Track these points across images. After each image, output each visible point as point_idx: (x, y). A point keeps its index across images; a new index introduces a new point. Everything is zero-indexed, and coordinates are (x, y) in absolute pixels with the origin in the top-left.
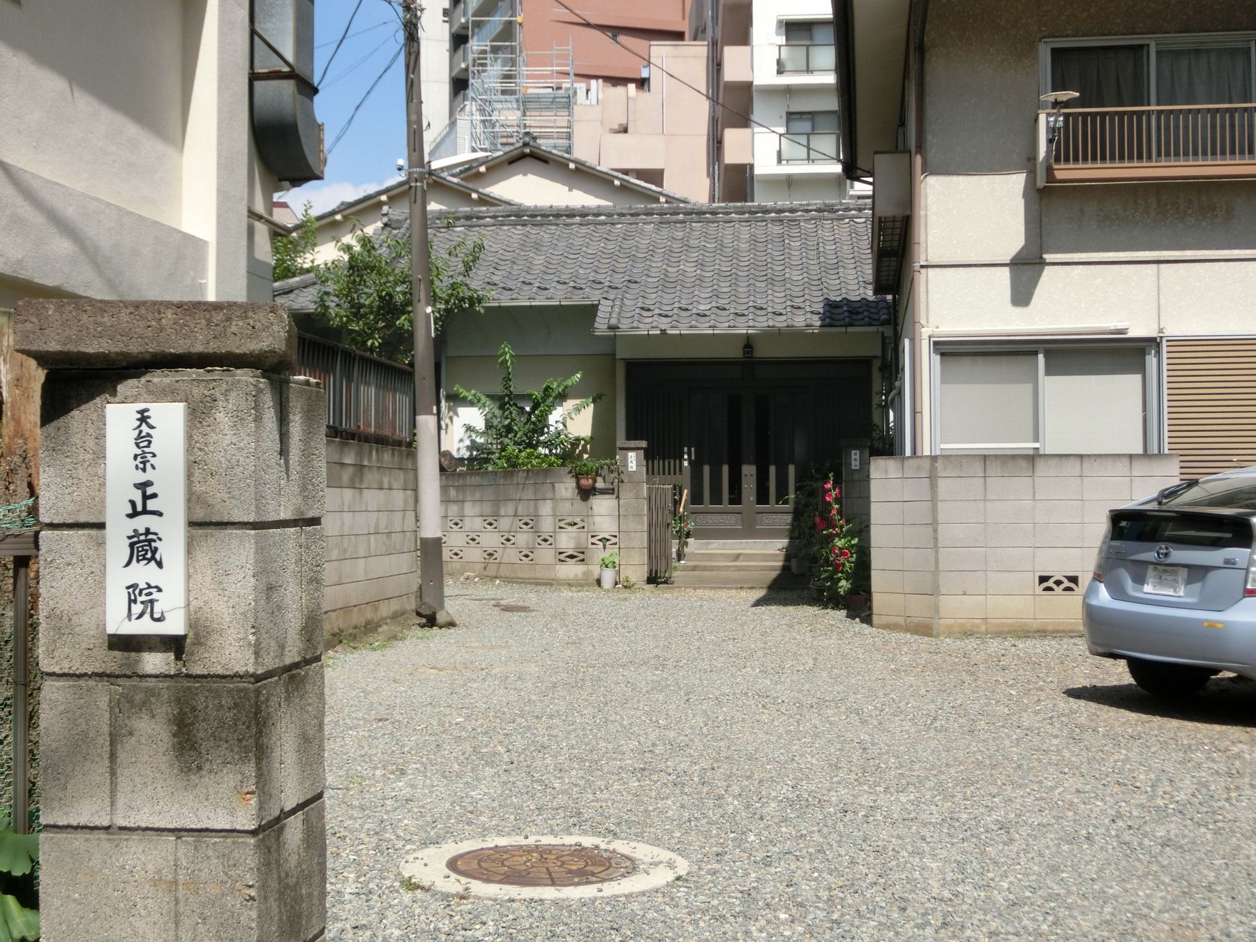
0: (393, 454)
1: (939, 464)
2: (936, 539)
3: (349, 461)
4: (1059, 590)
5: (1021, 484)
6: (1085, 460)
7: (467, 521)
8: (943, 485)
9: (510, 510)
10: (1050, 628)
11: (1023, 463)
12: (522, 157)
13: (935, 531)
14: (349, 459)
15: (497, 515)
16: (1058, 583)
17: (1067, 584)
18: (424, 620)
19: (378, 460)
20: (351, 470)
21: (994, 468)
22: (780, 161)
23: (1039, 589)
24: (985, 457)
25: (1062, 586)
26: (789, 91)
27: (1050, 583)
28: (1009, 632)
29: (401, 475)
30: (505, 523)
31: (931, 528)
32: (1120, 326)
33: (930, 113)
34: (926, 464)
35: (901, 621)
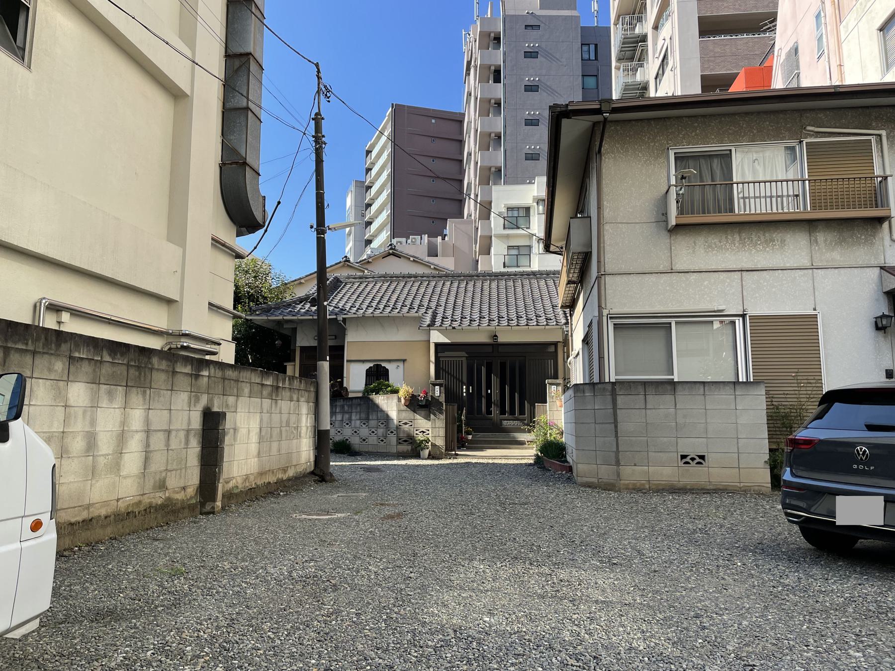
0: (301, 382)
1: (617, 387)
2: (616, 432)
3: (268, 383)
4: (693, 464)
5: (669, 398)
6: (706, 385)
7: (353, 422)
8: (620, 400)
9: (374, 417)
10: (689, 487)
11: (669, 387)
12: (390, 254)
13: (616, 427)
14: (269, 382)
15: (368, 419)
16: (693, 459)
17: (698, 460)
18: (317, 478)
19: (290, 384)
20: (270, 389)
21: (650, 390)
22: (504, 267)
23: (681, 464)
24: (645, 382)
25: (696, 461)
26: (508, 237)
27: (688, 459)
28: (663, 489)
29: (306, 394)
30: (373, 423)
31: (151, 448)
32: (721, 308)
33: (605, 189)
34: (609, 387)
35: (595, 480)
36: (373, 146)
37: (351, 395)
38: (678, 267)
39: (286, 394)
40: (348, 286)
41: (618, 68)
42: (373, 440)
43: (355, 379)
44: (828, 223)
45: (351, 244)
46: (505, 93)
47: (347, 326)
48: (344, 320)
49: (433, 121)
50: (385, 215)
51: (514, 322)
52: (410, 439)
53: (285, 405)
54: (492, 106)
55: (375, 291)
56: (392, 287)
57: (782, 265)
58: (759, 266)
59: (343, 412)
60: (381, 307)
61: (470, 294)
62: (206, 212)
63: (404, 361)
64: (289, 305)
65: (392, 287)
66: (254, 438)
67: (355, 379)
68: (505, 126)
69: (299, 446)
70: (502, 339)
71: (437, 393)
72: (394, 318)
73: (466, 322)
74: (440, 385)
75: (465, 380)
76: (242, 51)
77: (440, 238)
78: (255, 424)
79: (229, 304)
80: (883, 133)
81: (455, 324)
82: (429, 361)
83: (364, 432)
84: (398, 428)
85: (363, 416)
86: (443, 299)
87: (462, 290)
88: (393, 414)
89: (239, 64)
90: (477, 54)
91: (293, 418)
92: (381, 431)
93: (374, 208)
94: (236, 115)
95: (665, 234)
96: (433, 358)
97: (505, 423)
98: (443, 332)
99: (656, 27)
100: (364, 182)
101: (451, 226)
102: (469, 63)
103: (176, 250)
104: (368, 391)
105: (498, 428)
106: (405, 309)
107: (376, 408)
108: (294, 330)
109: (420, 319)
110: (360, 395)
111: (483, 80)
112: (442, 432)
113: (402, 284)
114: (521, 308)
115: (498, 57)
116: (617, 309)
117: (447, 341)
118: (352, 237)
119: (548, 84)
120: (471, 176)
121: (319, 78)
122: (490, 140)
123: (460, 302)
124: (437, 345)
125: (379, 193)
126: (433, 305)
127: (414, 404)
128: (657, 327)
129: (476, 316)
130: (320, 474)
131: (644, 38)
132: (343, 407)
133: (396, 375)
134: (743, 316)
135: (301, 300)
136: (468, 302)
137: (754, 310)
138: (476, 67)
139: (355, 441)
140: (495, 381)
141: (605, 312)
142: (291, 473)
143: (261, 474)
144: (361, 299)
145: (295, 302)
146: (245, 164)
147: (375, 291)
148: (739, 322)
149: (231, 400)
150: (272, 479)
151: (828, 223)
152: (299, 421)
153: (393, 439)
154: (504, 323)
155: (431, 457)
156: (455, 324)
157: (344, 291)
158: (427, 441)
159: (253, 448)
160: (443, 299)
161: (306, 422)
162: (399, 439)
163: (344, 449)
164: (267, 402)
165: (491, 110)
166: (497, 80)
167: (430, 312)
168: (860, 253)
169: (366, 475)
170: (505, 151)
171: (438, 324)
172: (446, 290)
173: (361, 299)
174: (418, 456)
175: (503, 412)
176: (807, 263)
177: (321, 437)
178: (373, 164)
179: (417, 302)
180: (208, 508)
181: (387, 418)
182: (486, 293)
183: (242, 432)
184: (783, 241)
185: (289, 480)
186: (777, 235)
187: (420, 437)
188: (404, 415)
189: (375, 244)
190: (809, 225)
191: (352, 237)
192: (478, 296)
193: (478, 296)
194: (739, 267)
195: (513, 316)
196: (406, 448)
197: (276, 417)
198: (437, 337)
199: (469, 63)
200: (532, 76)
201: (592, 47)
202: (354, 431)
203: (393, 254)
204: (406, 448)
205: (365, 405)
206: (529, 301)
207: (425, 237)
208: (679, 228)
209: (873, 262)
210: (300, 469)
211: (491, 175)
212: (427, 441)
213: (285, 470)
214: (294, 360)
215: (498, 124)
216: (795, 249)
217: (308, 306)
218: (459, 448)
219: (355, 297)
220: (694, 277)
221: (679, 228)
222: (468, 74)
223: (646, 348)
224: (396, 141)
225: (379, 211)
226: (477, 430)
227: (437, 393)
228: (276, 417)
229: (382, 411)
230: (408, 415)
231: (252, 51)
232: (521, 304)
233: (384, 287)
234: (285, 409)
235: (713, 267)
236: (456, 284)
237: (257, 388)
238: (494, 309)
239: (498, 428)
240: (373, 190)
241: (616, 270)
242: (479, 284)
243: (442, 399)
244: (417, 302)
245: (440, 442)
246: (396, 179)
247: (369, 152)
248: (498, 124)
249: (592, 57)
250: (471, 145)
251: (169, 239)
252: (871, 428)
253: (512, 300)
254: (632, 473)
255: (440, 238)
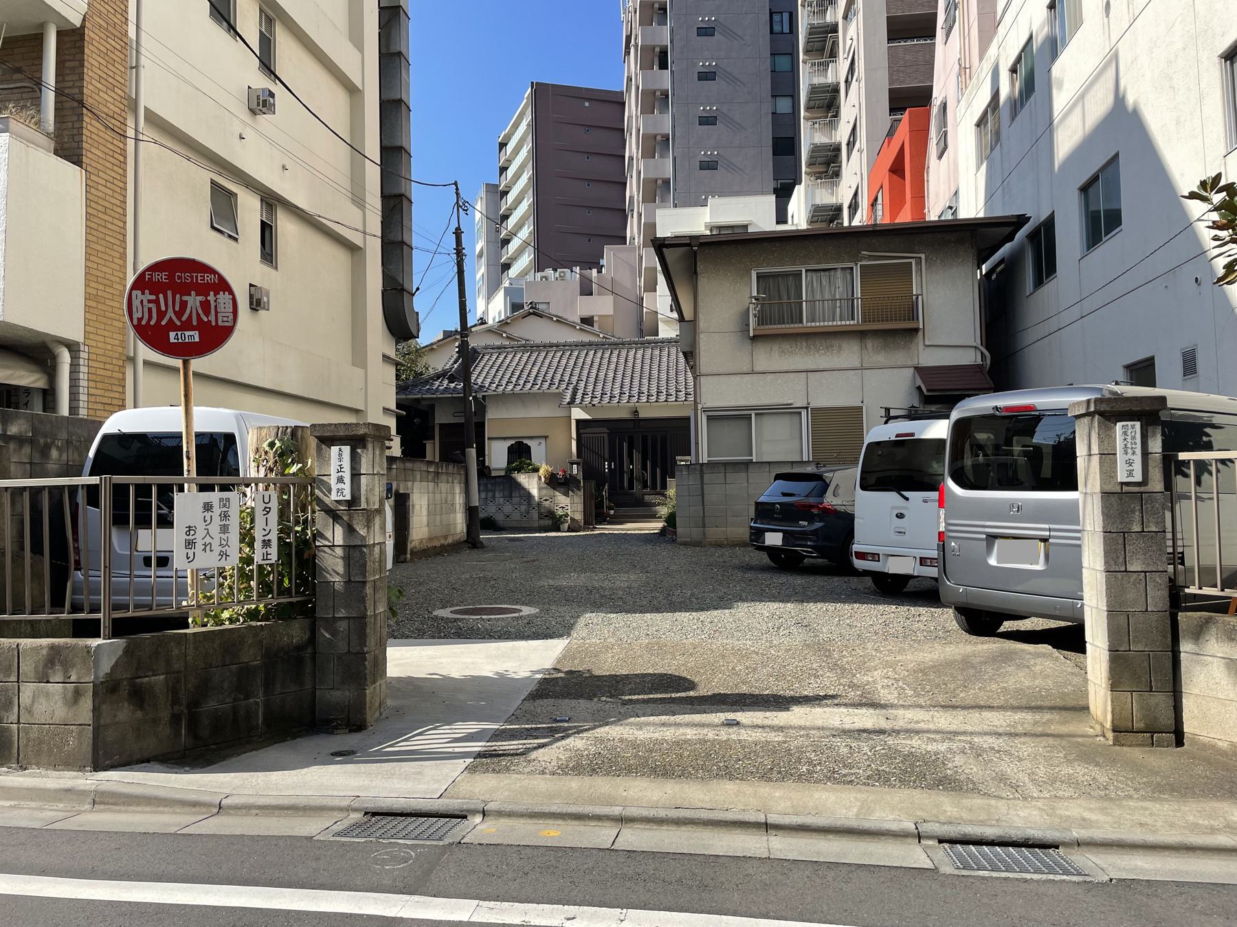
5: (743, 475)
11: (743, 466)
12: (530, 314)
15: (511, 497)
30: (515, 500)
36: (508, 137)
37: (494, 474)
38: (757, 369)
39: (444, 478)
40: (487, 357)
41: (804, 62)
42: (516, 516)
43: (498, 456)
44: (876, 333)
45: (483, 270)
46: (673, 83)
47: (487, 403)
48: (484, 397)
49: (587, 104)
50: (526, 232)
51: (653, 398)
52: (551, 514)
53: (444, 486)
54: (655, 101)
55: (514, 364)
56: (533, 358)
57: (838, 366)
58: (821, 367)
59: (487, 491)
60: (522, 382)
61: (613, 366)
62: (378, 340)
63: (546, 437)
64: (427, 382)
65: (533, 358)
66: (425, 512)
67: (498, 456)
68: (674, 127)
69: (455, 519)
70: (642, 415)
71: (575, 472)
72: (535, 395)
73: (606, 399)
74: (578, 464)
75: (607, 456)
76: (396, 192)
77: (594, 271)
78: (424, 502)
79: (393, 407)
80: (923, 256)
81: (596, 401)
82: (571, 438)
83: (508, 508)
84: (539, 504)
85: (507, 493)
86: (585, 372)
87: (605, 361)
88: (535, 492)
89: (395, 205)
90: (638, 31)
91: (450, 497)
92: (523, 508)
93: (512, 222)
94: (395, 248)
95: (748, 346)
96: (574, 435)
97: (646, 497)
98: (585, 409)
99: (845, 17)
100: (497, 186)
101: (610, 255)
102: (628, 38)
103: (360, 371)
104: (509, 470)
105: (640, 503)
106: (546, 385)
107: (519, 486)
108: (432, 407)
109: (560, 396)
110: (503, 473)
111: (645, 66)
112: (580, 507)
113: (543, 354)
114: (663, 383)
115: (663, 35)
116: (708, 405)
117: (589, 417)
118: (484, 260)
119: (728, 69)
120: (633, 189)
121: (457, 194)
122: (655, 145)
123: (602, 375)
124: (578, 421)
125: (518, 201)
126: (574, 379)
127: (553, 482)
128: (740, 417)
129: (617, 392)
130: (471, 542)
131: (834, 28)
132: (486, 485)
133: (538, 451)
134: (807, 408)
135: (438, 376)
136: (611, 375)
137: (815, 404)
138: (636, 46)
139: (499, 518)
140: (637, 456)
141: (700, 406)
142: (450, 540)
143: (430, 539)
144: (500, 373)
145: (432, 378)
146: (403, 290)
147: (514, 364)
148: (804, 413)
149: (410, 484)
150: (438, 544)
151: (876, 333)
152: (454, 499)
153: (535, 515)
154: (644, 399)
155: (570, 530)
156: (596, 401)
157: (482, 364)
158: (567, 515)
159: (425, 519)
160: (585, 372)
161: (459, 500)
162: (540, 514)
163: (490, 525)
164: (431, 485)
165: (657, 105)
166: (663, 65)
167: (571, 387)
168: (900, 357)
169: (511, 544)
170: (674, 159)
171: (578, 401)
172: (589, 360)
173: (500, 373)
174: (558, 530)
175: (645, 486)
176: (858, 365)
177: (471, 512)
178: (509, 161)
179: (558, 377)
180: (402, 558)
181: (529, 496)
182: (630, 364)
183: (417, 507)
184: (840, 348)
185: (449, 545)
186: (835, 342)
187: (560, 512)
188: (544, 492)
189: (513, 272)
190: (860, 335)
191: (484, 260)
192: (621, 367)
193: (621, 367)
194: (805, 368)
195: (654, 392)
196: (548, 522)
197: (438, 496)
198: (578, 414)
199: (628, 38)
200: (707, 60)
201: (786, 16)
202: (499, 508)
203: (534, 314)
204: (548, 522)
205: (508, 484)
206: (672, 373)
207: (577, 269)
208: (755, 338)
209: (910, 363)
210: (456, 538)
211: (657, 190)
212: (567, 515)
213: (446, 537)
214: (433, 438)
215: (665, 123)
216: (849, 354)
217: (446, 382)
218: (600, 523)
219: (493, 371)
220: (770, 376)
221: (755, 338)
222: (628, 53)
223: (730, 433)
224: (537, 128)
225: (519, 226)
226: (618, 505)
227: (575, 472)
228: (438, 496)
229: (525, 489)
230: (549, 492)
231: (403, 191)
232: (664, 376)
233: (525, 358)
234: (444, 490)
235: (785, 368)
236: (599, 355)
237: (425, 474)
238: (636, 383)
239: (640, 503)
240: (511, 197)
241: (709, 372)
242: (624, 353)
243: (580, 477)
244: (558, 377)
245: (579, 516)
246: (540, 184)
247: (503, 145)
248: (665, 123)
249: (786, 29)
250: (632, 148)
251: (354, 364)
252: (784, 495)
253: (655, 373)
254: (714, 533)
255: (594, 271)
